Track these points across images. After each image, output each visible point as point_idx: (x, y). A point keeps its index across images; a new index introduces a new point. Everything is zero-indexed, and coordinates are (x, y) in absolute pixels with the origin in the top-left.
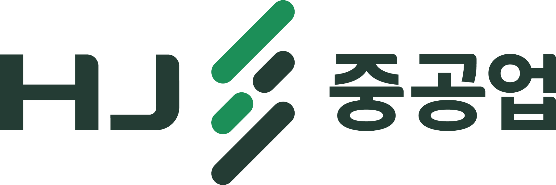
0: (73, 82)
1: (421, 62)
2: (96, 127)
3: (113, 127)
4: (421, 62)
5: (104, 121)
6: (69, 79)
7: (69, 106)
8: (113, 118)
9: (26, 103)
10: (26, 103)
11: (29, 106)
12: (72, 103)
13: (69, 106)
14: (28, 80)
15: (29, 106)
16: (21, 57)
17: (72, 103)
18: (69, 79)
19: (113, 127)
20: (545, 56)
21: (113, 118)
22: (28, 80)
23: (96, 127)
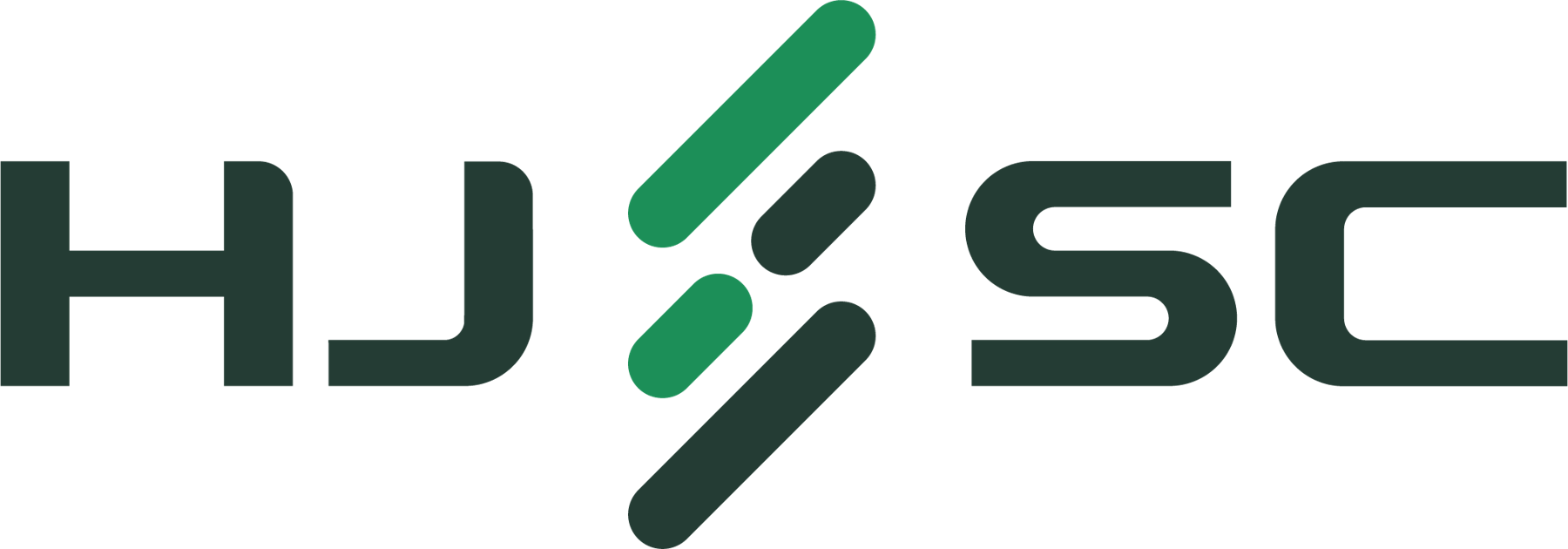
0: (76, 244)
1: (979, 378)
2: (285, 378)
3: (336, 378)
4: (979, 378)
5: (310, 358)
6: (206, 233)
7: (206, 314)
8: (336, 348)
9: (78, 306)
10: (78, 306)
11: (86, 314)
12: (214, 306)
13: (206, 314)
14: (85, 234)
15: (86, 314)
16: (229, 167)
17: (214, 306)
18: (206, 233)
19: (336, 378)
20: (53, 370)
21: (336, 348)
22: (85, 234)
23: (285, 378)
